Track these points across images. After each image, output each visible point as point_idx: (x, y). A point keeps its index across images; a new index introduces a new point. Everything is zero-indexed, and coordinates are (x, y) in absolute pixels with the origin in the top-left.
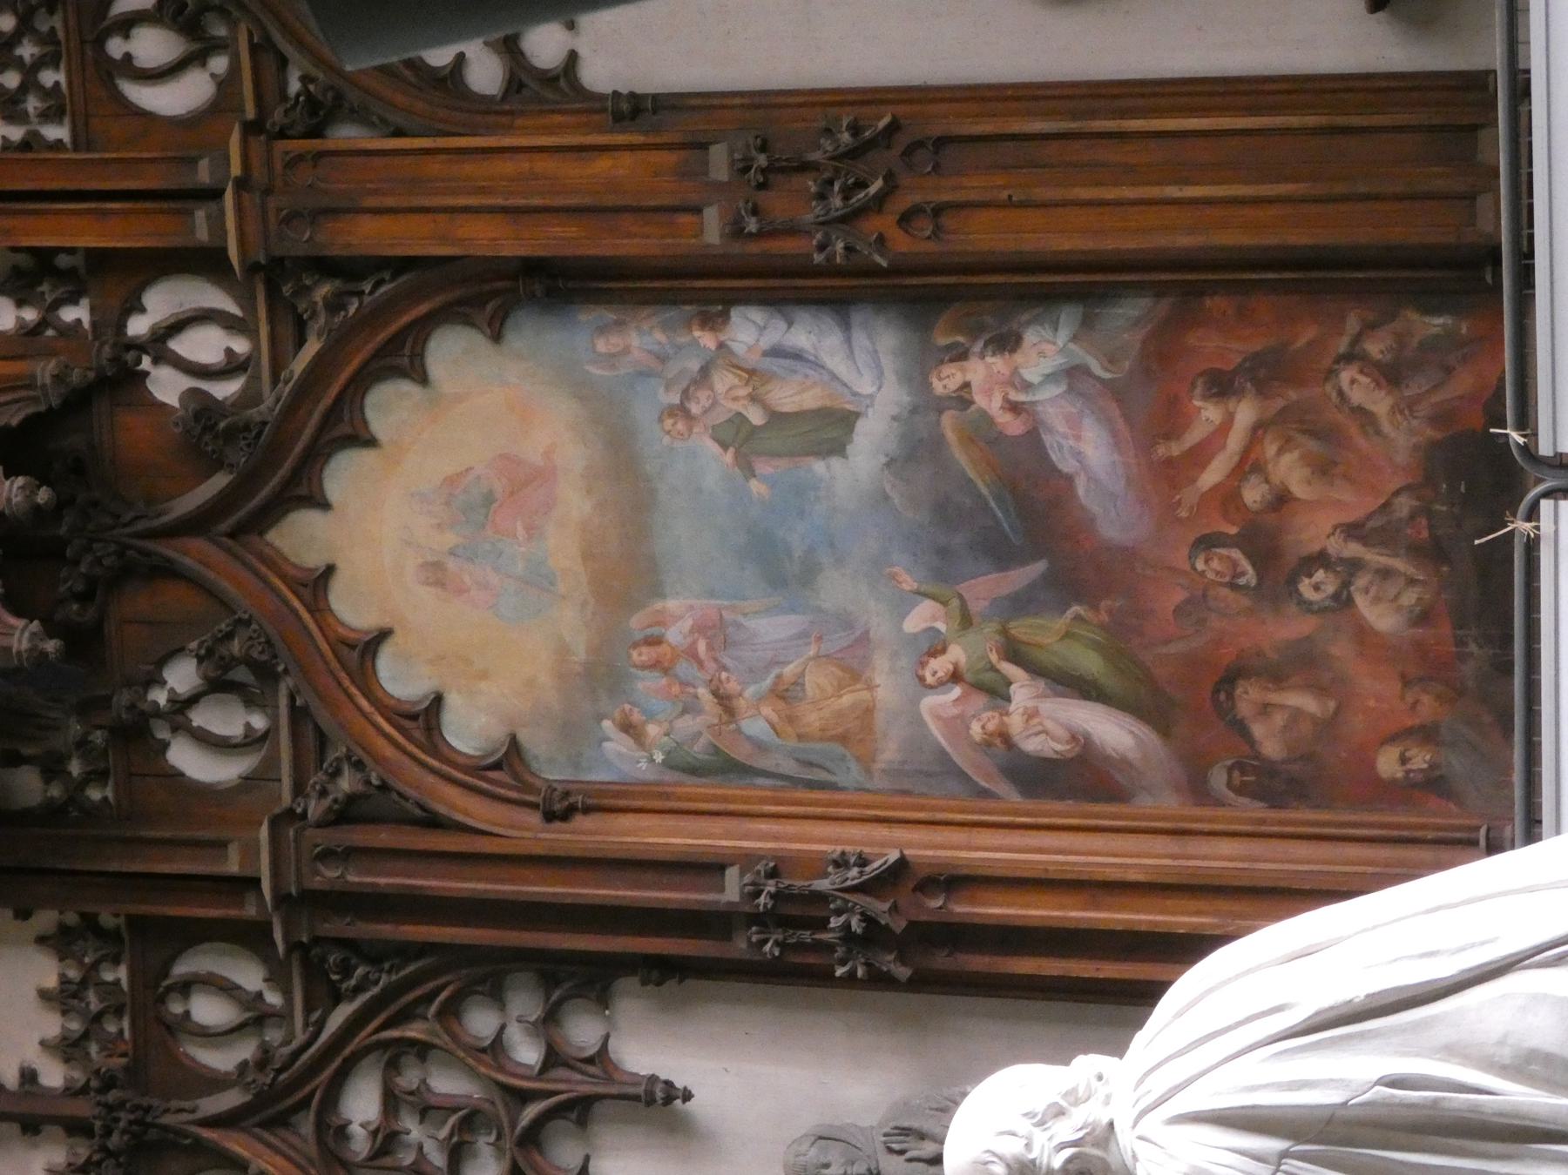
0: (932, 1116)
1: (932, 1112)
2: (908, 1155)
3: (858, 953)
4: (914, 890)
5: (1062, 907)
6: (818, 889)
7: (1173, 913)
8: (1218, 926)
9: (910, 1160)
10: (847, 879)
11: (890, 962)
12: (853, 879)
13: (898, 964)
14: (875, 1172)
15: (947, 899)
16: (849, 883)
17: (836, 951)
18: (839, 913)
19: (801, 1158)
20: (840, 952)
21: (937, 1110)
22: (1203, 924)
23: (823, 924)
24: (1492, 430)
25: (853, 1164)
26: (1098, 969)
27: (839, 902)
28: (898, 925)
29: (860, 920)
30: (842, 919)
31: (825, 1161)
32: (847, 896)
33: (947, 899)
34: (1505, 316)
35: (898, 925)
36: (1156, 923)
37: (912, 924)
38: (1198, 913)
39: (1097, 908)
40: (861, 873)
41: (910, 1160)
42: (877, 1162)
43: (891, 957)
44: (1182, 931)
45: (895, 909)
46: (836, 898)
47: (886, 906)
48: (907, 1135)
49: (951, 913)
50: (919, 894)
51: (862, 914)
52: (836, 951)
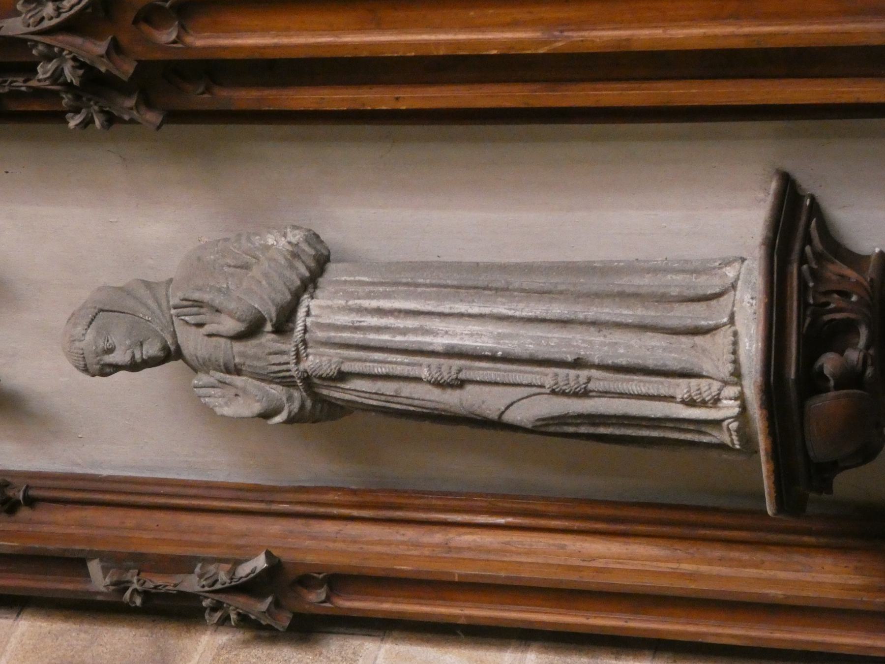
0: (232, 275)
1: (232, 270)
2: (208, 329)
3: (89, 100)
4: (136, 22)
5: (331, 29)
6: (10, 34)
7: (479, 28)
8: (545, 43)
9: (210, 335)
10: (42, 19)
11: (131, 109)
12: (51, 18)
13: (143, 109)
14: (172, 348)
15: (183, 28)
16: (46, 24)
17: (63, 98)
18: (48, 58)
19: (77, 344)
20: (66, 100)
21: (235, 267)
22: (520, 41)
23: (30, 69)
24: (815, 220)
25: (141, 345)
26: (397, 99)
27: (41, 47)
28: (126, 69)
29: (74, 67)
30: (51, 66)
31: (107, 345)
32: (47, 40)
33: (183, 28)
34: (767, 500)
35: (126, 69)
36: (458, 43)
37: (142, 66)
38: (514, 25)
39: (380, 26)
40: (58, 10)
41: (210, 335)
42: (174, 335)
43: (130, 102)
44: (494, 52)
45: (116, 48)
46: (36, 43)
47: (100, 48)
48: (201, 307)
49: (189, 48)
50: (145, 27)
51: (74, 59)
52: (63, 98)
